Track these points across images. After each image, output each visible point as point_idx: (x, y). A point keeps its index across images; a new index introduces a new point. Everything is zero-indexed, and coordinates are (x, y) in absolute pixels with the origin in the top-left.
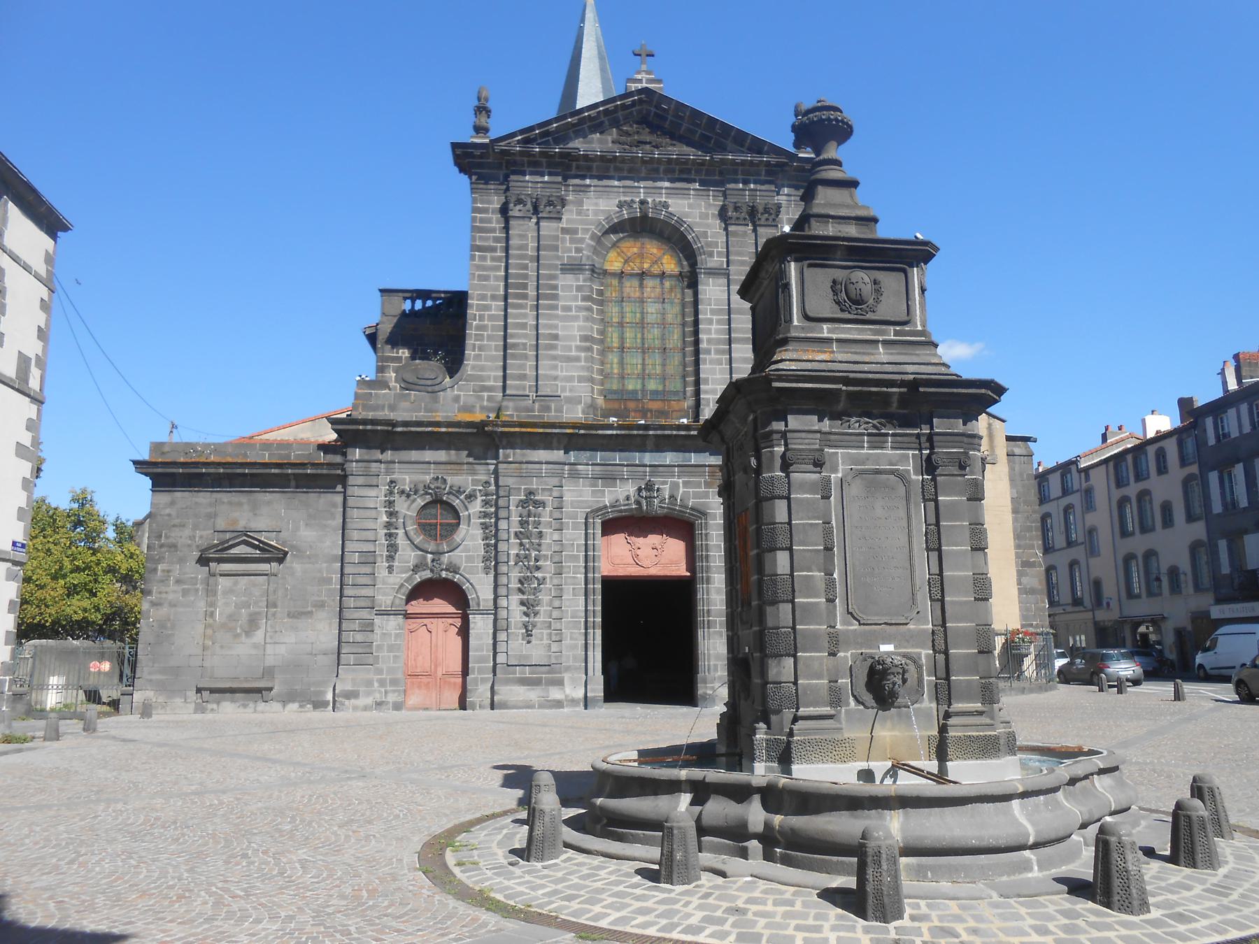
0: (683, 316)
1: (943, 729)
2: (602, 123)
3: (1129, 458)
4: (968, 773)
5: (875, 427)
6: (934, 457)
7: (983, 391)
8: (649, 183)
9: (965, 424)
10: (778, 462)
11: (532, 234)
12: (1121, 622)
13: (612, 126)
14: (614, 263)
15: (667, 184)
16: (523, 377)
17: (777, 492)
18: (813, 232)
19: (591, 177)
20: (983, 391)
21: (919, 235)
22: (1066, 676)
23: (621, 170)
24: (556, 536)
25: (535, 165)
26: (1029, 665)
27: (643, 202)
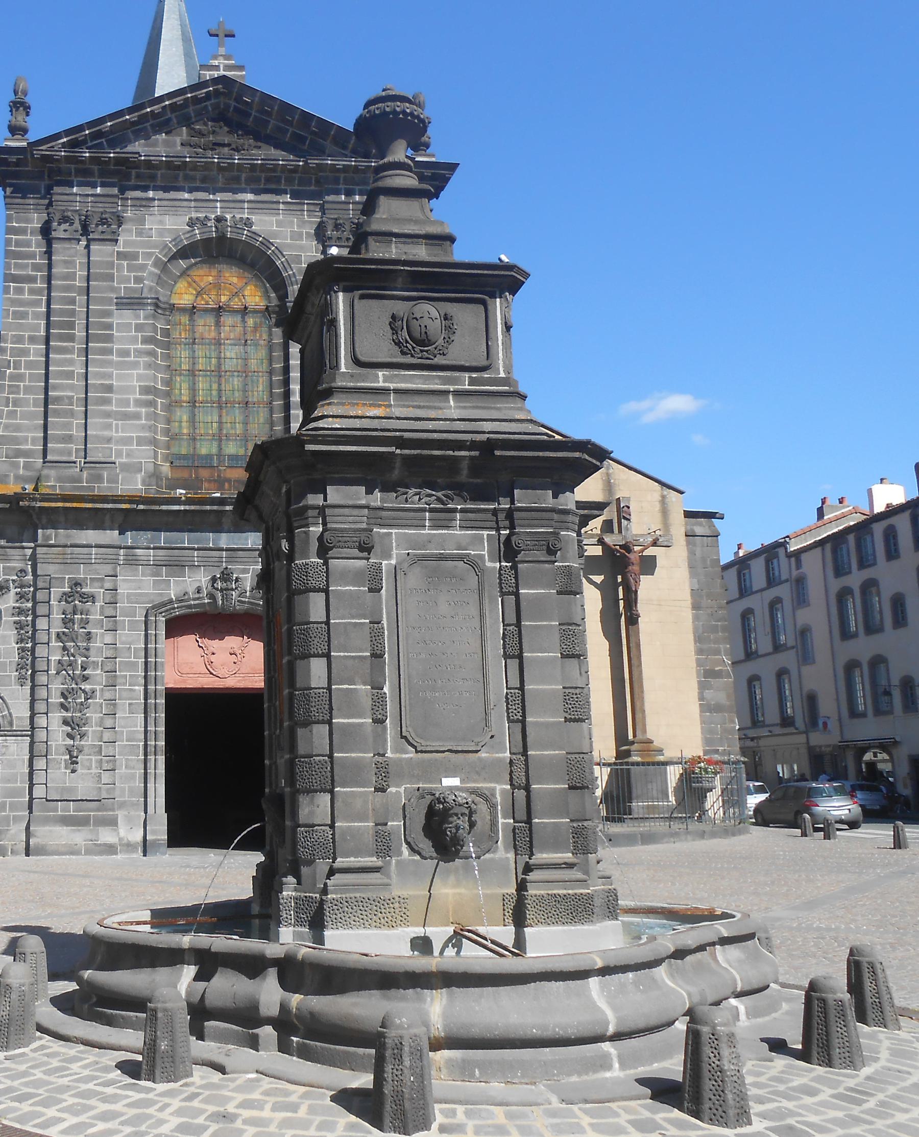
0: (271, 360)
1: (522, 887)
2: (169, 120)
3: (851, 538)
4: (548, 943)
5: (439, 500)
6: (513, 538)
7: (577, 455)
8: (228, 196)
9: (555, 496)
10: (314, 546)
11: (80, 260)
12: (843, 748)
13: (180, 124)
14: (184, 296)
15: (250, 196)
16: (69, 439)
17: (313, 583)
18: (370, 255)
19: (155, 189)
20: (577, 455)
21: (503, 258)
22: (763, 817)
23: (193, 179)
24: (108, 639)
25: (84, 174)
26: (713, 802)
27: (219, 220)
